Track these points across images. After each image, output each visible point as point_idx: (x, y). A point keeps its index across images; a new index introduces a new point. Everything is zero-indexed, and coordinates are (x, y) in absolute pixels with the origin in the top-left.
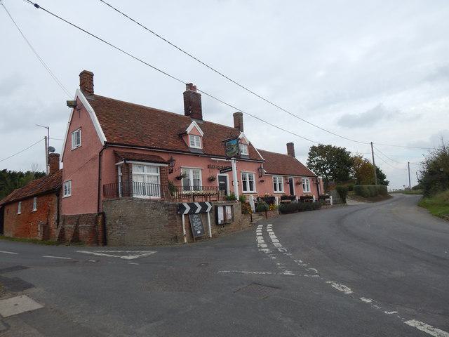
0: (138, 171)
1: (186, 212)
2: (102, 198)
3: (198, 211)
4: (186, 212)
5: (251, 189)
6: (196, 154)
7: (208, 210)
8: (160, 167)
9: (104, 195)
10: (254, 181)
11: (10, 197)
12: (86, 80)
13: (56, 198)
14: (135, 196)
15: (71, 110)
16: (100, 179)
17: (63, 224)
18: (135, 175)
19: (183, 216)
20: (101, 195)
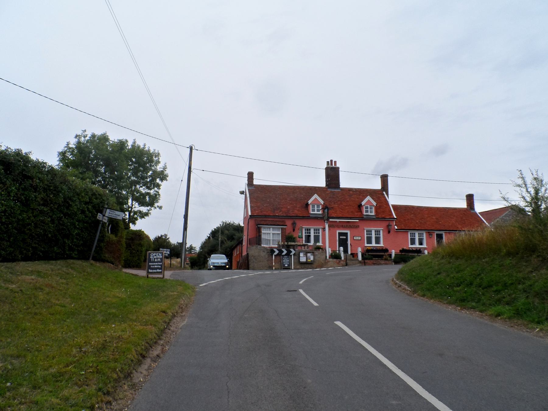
0: (268, 231)
1: (275, 254)
2: (248, 246)
3: (284, 254)
4: (275, 254)
5: (421, 243)
6: (316, 218)
7: (292, 254)
8: (282, 228)
9: (250, 244)
10: (381, 236)
11: (144, 253)
12: (250, 176)
13: (241, 245)
14: (262, 245)
15: (72, 407)
16: (248, 235)
17: (3, 188)
18: (264, 233)
19: (274, 256)
20: (248, 244)
